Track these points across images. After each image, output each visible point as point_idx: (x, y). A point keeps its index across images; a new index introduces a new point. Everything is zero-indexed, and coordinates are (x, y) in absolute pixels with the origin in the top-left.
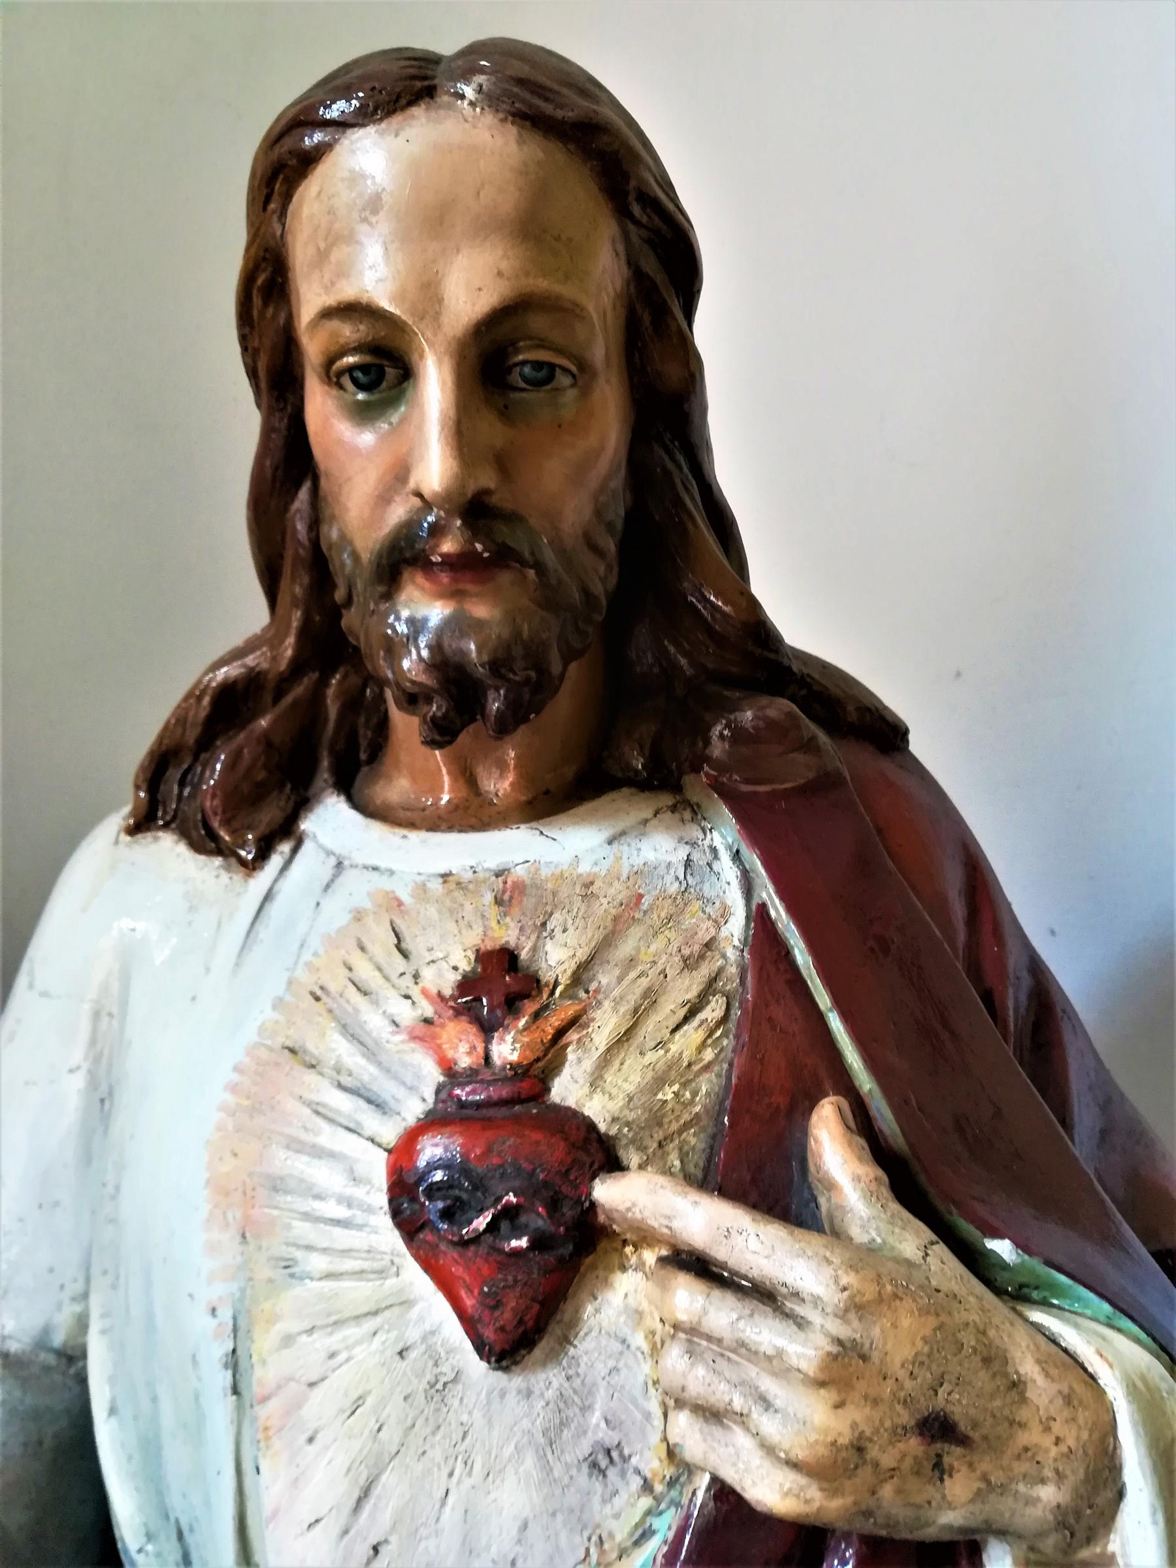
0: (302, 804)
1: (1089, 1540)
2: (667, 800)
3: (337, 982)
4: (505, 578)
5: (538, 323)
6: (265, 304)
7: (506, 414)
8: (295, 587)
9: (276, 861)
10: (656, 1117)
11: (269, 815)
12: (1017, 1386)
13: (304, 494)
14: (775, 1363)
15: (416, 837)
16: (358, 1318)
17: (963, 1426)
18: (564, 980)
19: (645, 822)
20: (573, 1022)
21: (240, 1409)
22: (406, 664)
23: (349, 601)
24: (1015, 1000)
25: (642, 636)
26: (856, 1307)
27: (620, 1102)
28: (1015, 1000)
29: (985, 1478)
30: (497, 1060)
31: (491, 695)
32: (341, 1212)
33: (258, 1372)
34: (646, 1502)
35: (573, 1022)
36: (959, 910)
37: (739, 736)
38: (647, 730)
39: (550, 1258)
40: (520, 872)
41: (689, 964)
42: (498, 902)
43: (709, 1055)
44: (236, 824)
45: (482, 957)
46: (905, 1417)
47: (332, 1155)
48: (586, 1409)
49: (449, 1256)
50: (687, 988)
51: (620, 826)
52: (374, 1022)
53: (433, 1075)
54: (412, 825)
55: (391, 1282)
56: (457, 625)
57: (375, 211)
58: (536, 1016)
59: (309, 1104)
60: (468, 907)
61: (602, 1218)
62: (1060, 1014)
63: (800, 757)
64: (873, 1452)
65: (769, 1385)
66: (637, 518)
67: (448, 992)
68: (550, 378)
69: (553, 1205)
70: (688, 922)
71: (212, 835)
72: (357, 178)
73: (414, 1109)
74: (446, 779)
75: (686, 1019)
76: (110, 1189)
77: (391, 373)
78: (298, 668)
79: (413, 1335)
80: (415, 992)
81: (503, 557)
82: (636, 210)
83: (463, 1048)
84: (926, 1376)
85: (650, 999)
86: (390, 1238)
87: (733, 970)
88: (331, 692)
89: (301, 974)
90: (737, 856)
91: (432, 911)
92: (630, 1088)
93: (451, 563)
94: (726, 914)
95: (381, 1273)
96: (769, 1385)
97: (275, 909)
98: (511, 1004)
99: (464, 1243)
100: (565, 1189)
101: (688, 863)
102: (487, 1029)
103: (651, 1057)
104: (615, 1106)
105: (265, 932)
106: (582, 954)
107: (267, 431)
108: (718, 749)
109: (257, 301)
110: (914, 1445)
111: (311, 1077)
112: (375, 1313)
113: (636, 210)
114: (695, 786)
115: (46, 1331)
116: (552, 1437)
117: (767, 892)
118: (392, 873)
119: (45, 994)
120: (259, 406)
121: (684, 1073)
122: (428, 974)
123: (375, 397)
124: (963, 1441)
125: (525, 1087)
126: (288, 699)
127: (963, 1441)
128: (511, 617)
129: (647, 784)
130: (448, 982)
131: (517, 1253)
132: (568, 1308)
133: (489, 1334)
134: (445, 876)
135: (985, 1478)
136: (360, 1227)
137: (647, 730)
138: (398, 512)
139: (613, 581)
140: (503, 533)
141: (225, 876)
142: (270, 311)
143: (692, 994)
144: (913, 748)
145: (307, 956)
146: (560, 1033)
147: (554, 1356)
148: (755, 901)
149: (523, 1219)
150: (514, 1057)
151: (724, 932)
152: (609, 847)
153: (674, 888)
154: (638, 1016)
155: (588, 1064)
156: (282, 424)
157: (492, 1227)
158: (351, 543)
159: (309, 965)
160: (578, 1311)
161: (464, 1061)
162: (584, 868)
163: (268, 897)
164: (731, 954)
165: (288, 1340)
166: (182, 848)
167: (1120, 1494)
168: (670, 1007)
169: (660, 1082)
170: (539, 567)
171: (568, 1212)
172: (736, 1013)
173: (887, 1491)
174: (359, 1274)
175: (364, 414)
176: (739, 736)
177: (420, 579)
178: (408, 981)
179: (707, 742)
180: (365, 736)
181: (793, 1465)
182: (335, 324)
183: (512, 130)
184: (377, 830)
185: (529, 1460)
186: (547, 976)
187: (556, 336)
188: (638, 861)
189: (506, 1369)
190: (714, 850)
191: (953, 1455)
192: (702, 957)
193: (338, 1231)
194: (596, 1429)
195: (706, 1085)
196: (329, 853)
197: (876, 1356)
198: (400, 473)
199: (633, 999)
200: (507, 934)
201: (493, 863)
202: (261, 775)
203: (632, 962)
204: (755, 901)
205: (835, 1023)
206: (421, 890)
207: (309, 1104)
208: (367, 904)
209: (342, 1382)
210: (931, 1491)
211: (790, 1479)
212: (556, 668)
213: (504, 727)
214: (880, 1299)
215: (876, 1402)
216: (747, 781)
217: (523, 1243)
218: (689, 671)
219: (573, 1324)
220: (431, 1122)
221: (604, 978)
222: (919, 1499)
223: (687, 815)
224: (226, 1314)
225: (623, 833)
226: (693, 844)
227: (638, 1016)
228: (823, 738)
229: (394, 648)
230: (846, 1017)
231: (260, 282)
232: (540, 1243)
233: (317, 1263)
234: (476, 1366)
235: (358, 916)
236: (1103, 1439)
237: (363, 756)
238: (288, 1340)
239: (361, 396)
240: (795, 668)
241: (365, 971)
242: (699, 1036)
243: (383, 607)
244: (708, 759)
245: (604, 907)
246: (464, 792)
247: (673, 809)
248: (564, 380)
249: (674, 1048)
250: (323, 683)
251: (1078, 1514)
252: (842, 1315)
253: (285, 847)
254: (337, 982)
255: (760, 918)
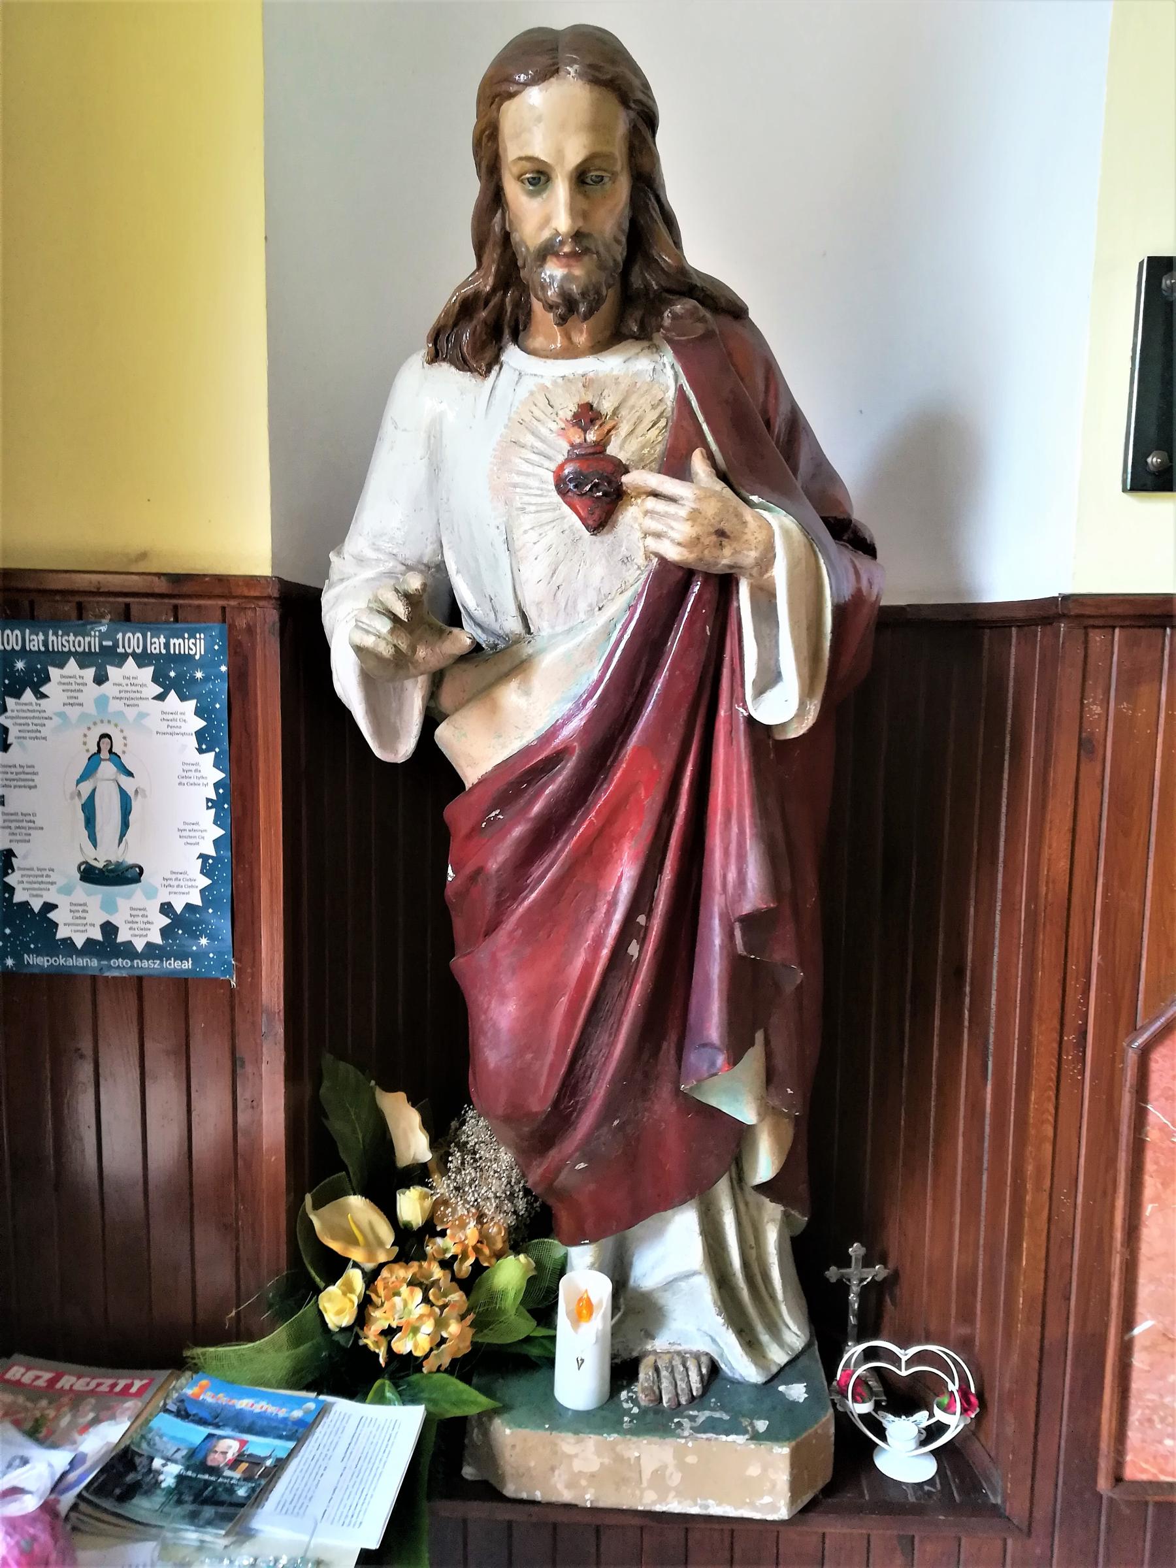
0: (500, 350)
1: (767, 571)
2: (646, 344)
3: (528, 417)
4: (586, 258)
5: (597, 162)
6: (488, 141)
7: (586, 195)
8: (492, 254)
9: (494, 373)
10: (642, 459)
11: (489, 354)
12: (745, 523)
13: (499, 215)
14: (674, 517)
15: (550, 362)
16: (547, 523)
17: (728, 533)
18: (610, 414)
19: (638, 354)
20: (613, 427)
21: (510, 554)
22: (549, 293)
23: (524, 267)
24: (779, 424)
25: (636, 269)
26: (699, 499)
27: (630, 453)
28: (779, 424)
29: (735, 549)
30: (588, 440)
31: (581, 305)
32: (539, 492)
33: (516, 543)
34: (639, 572)
35: (613, 427)
36: (761, 386)
37: (675, 317)
38: (638, 314)
39: (608, 499)
40: (591, 374)
41: (654, 407)
42: (584, 386)
43: (660, 438)
44: (477, 358)
45: (580, 406)
46: (712, 530)
47: (534, 475)
48: (621, 546)
49: (576, 500)
50: (653, 415)
51: (628, 355)
52: (544, 431)
53: (566, 447)
54: (547, 357)
55: (558, 512)
56: (567, 278)
57: (540, 122)
58: (601, 425)
59: (524, 459)
60: (573, 388)
61: (624, 488)
62: (801, 429)
63: (699, 325)
64: (702, 540)
65: (674, 524)
66: (633, 222)
67: (569, 419)
68: (602, 180)
69: (609, 483)
70: (654, 392)
71: (465, 361)
72: (532, 107)
73: (561, 459)
74: (559, 338)
75: (653, 426)
76: (445, 500)
77: (543, 178)
78: (494, 290)
79: (566, 527)
80: (557, 419)
81: (586, 251)
82: (633, 105)
83: (577, 436)
84: (718, 519)
85: (640, 420)
86: (557, 499)
87: (670, 409)
88: (508, 300)
89: (513, 415)
90: (673, 367)
91: (560, 391)
92: (633, 449)
93: (566, 255)
94: (667, 389)
95: (554, 509)
96: (674, 524)
97: (498, 392)
98: (592, 421)
99: (582, 495)
100: (613, 479)
101: (654, 369)
102: (585, 431)
103: (640, 439)
104: (628, 455)
105: (495, 401)
106: (616, 405)
107: (483, 192)
108: (667, 322)
109: (484, 139)
110: (714, 538)
111: (523, 451)
112: (553, 521)
113: (633, 105)
114: (658, 337)
115: (421, 557)
116: (611, 553)
117: (683, 381)
118: (542, 376)
119: (405, 430)
120: (480, 177)
121: (652, 444)
122: (561, 413)
123: (537, 188)
124: (728, 537)
125: (598, 449)
126: (492, 304)
127: (728, 537)
128: (588, 274)
129: (637, 338)
130: (569, 415)
131: (598, 497)
132: (614, 517)
133: (590, 522)
134: (563, 377)
135: (735, 549)
136: (546, 496)
137: (638, 314)
138: (546, 234)
139: (625, 254)
140: (585, 243)
141: (473, 380)
142: (489, 144)
143: (654, 418)
144: (750, 316)
145: (514, 409)
146: (609, 431)
147: (610, 531)
148: (679, 383)
149: (600, 487)
150: (594, 439)
151: (667, 395)
152: (11, 750)
153: (649, 379)
154: (636, 425)
155: (619, 441)
156: (492, 186)
157: (591, 489)
158: (525, 243)
159: (516, 413)
160: (617, 517)
161: (578, 441)
162: (615, 373)
163: (493, 388)
164: (669, 404)
165: (525, 532)
166: (453, 369)
167: (775, 556)
168: (647, 423)
169: (643, 448)
170: (598, 253)
171: (614, 485)
172: (670, 424)
173: (706, 552)
174: (546, 510)
175: (532, 194)
176: (675, 317)
177: (555, 260)
178: (554, 416)
179: (662, 319)
180: (522, 318)
181: (679, 544)
182: (524, 162)
183: (588, 87)
184: (533, 360)
185: (603, 561)
186: (603, 412)
187: (604, 165)
188: (635, 370)
189: (596, 535)
190: (664, 364)
191: (725, 542)
192: (658, 405)
193: (538, 498)
194: (624, 551)
195: (659, 449)
196: (515, 370)
197: (703, 513)
198: (547, 221)
199: (633, 421)
200: (589, 398)
201: (581, 372)
202: (484, 337)
203: (633, 407)
204: (679, 383)
205: (705, 427)
206: (555, 383)
207: (524, 459)
208: (535, 389)
209: (545, 542)
210: (719, 552)
211: (679, 549)
212: (604, 293)
213: (586, 317)
214: (705, 497)
215: (703, 525)
216: (678, 336)
217: (601, 494)
218: (656, 288)
219: (616, 522)
220: (567, 461)
221: (623, 412)
222: (715, 555)
223: (654, 350)
224: (503, 528)
225: (629, 359)
226: (656, 362)
227: (636, 425)
228: (708, 315)
229: (544, 287)
230: (708, 424)
231: (487, 133)
232: (605, 494)
233: (533, 508)
234: (586, 534)
235: (532, 393)
236: (770, 542)
237: (521, 328)
238: (525, 532)
239: (531, 188)
240: (699, 285)
241: (537, 413)
242: (658, 431)
243: (539, 270)
244: (662, 326)
245: (623, 386)
246: (566, 343)
247: (649, 348)
248: (606, 180)
249: (648, 436)
250: (505, 294)
251: (762, 560)
252: (694, 501)
253: (496, 368)
254: (528, 417)
255: (680, 390)
